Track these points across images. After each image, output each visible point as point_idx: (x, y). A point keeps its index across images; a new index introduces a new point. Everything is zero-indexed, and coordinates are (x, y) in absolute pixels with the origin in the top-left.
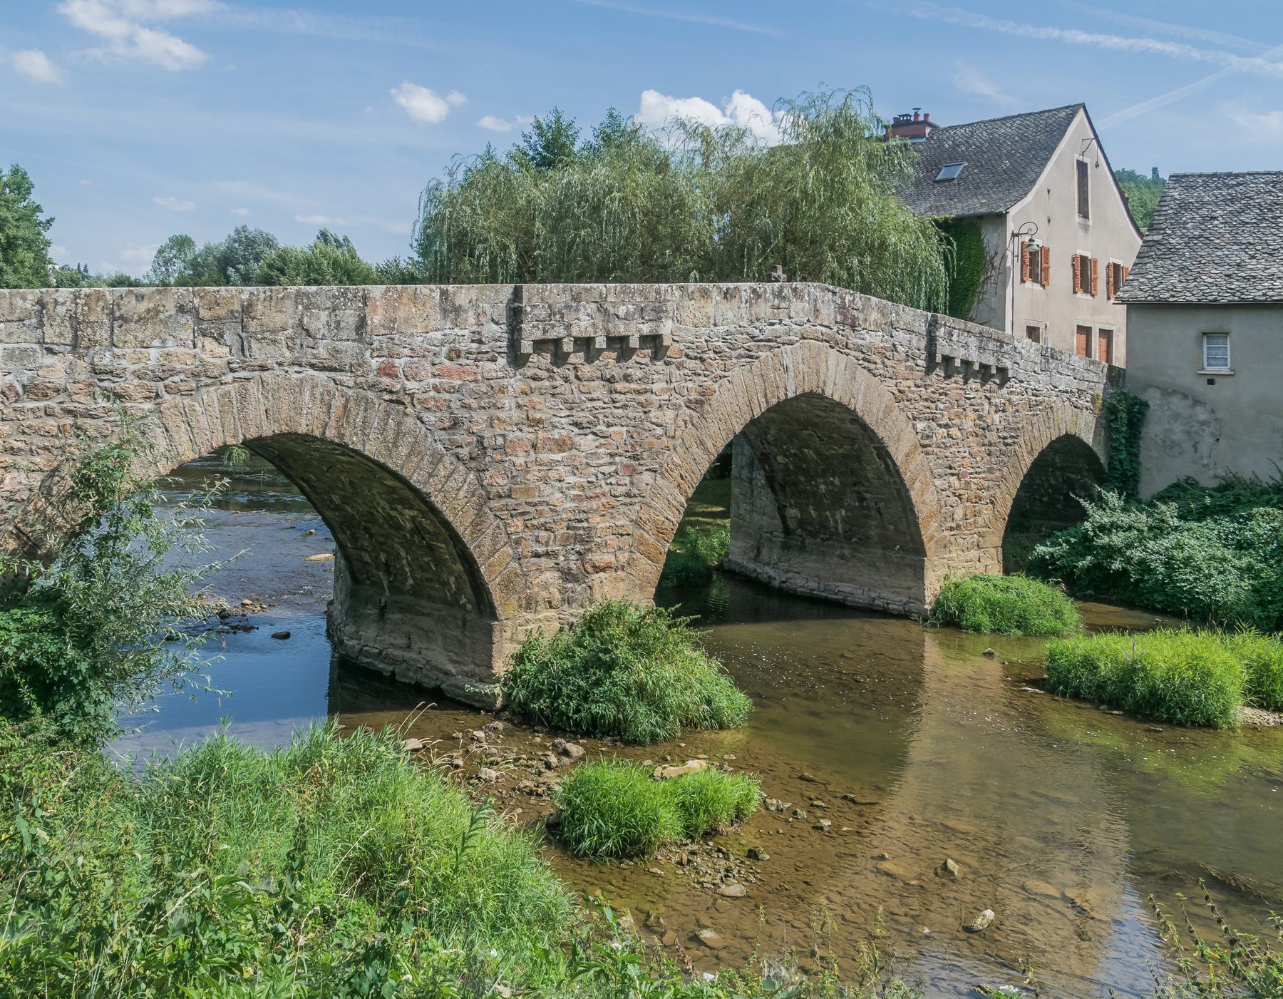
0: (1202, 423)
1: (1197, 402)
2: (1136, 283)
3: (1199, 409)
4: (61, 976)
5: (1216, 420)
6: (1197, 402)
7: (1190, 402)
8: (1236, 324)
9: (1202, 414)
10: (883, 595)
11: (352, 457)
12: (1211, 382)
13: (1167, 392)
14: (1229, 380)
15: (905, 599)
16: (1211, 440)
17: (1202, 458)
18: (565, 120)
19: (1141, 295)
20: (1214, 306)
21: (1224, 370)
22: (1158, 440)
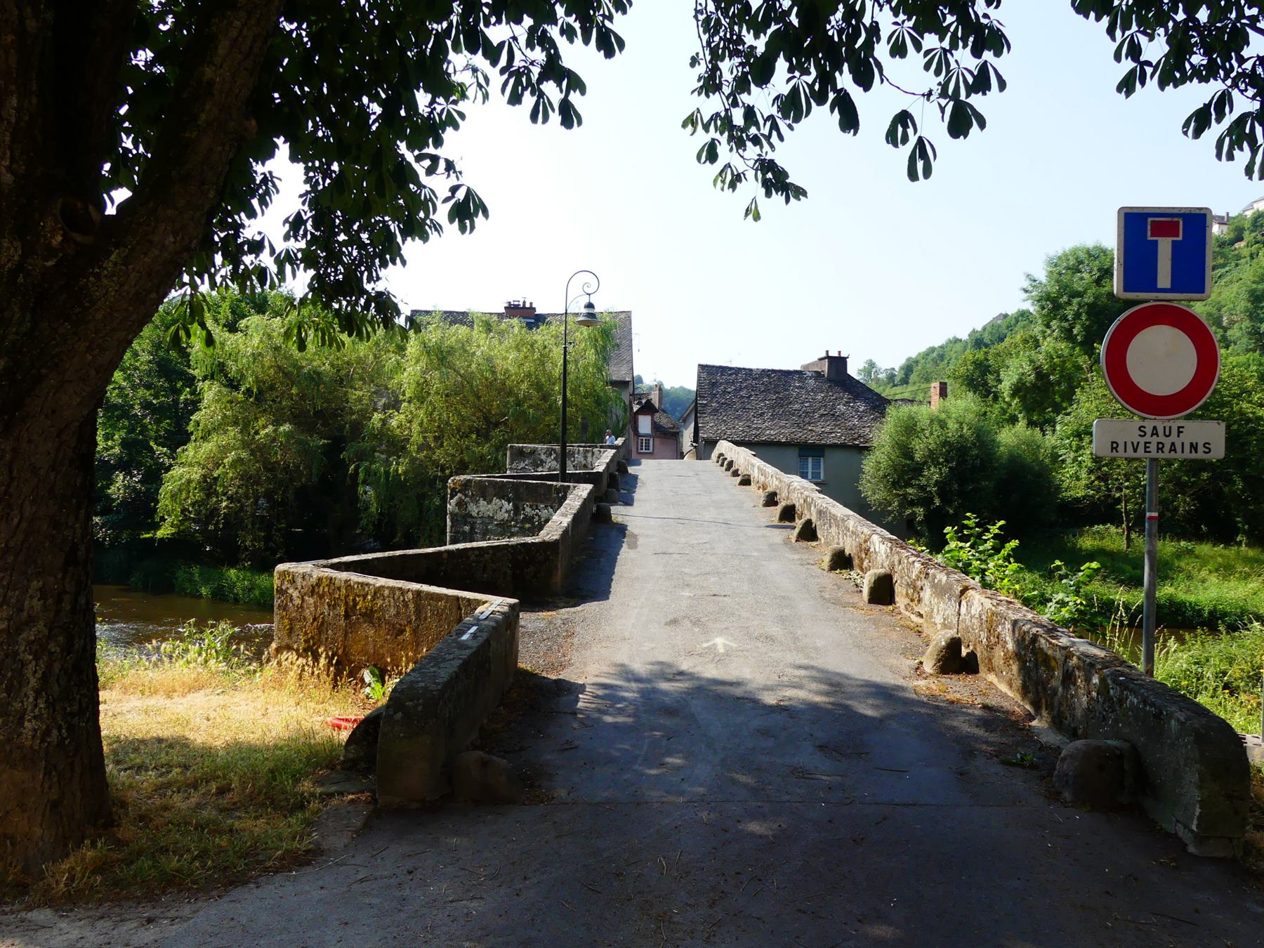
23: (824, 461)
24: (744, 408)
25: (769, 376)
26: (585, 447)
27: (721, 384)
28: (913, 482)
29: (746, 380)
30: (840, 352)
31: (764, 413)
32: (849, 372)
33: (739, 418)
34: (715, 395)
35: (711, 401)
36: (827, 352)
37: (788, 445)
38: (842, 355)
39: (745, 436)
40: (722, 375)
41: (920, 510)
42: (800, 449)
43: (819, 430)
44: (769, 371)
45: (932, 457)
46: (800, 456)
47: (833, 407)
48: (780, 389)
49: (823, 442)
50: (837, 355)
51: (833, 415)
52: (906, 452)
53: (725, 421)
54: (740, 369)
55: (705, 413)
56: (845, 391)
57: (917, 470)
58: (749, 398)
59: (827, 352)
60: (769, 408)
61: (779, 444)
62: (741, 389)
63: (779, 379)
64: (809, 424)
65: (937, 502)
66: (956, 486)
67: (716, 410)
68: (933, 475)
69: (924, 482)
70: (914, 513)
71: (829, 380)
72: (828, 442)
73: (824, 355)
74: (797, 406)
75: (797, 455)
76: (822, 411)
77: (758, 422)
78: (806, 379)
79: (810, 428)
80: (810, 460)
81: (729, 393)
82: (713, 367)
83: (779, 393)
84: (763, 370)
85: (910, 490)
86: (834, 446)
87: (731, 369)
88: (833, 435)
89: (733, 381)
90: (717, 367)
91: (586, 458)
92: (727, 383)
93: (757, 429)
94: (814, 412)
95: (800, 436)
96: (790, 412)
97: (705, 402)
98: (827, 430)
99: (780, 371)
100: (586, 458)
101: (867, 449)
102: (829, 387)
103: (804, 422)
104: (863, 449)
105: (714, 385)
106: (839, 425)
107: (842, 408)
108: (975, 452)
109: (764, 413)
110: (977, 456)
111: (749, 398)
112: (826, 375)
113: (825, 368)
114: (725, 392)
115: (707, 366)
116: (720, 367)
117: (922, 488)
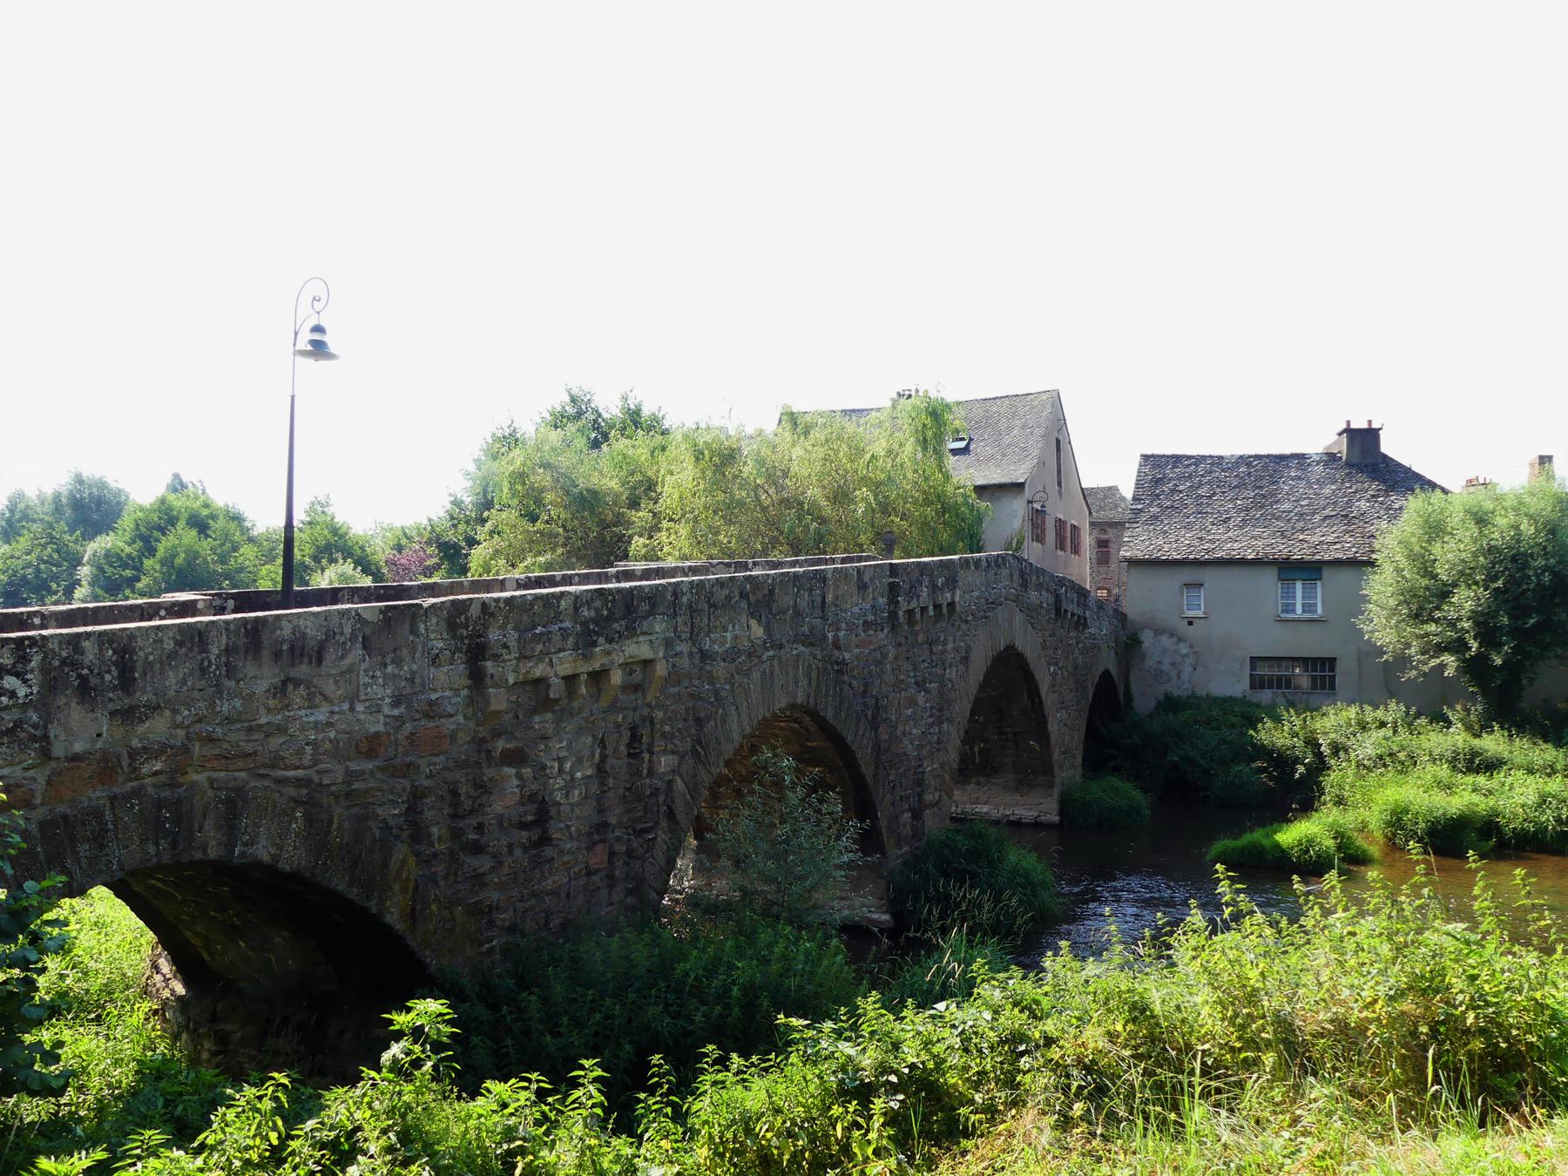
0: (1185, 656)
1: (1180, 639)
2: (1132, 544)
3: (1182, 645)
4: (1299, 474)
5: (1194, 652)
6: (1180, 639)
7: (1175, 639)
8: (1209, 576)
9: (1184, 649)
10: (1016, 812)
11: (1463, 1086)
12: (1190, 623)
13: (1159, 631)
14: (1202, 621)
15: (1036, 814)
16: (1190, 669)
17: (1183, 684)
18: (550, 409)
19: (1139, 555)
20: (1196, 563)
21: (1200, 613)
22: (1151, 670)
23: (1323, 587)
24: (1200, 513)
25: (1249, 465)
26: (660, 573)
27: (1170, 480)
28: (1437, 614)
29: (1211, 472)
30: (1370, 422)
31: (1229, 519)
32: (1382, 450)
33: (1189, 527)
34: (1158, 495)
35: (1150, 505)
36: (1348, 422)
37: (1258, 563)
38: (1374, 426)
39: (1191, 553)
40: (1174, 467)
41: (1449, 659)
42: (1280, 569)
43: (1316, 539)
44: (1250, 457)
45: (1465, 575)
46: (1280, 579)
47: (1349, 503)
48: (1264, 482)
49: (1317, 557)
50: (1365, 426)
51: (1346, 516)
52: (1426, 568)
53: (1165, 532)
54: (1204, 458)
55: (1137, 522)
56: (1374, 479)
57: (1444, 594)
58: (1210, 497)
59: (1348, 422)
60: (1240, 511)
61: (1243, 562)
62: (1200, 485)
63: (1265, 468)
64: (1302, 531)
65: (1474, 645)
66: (1505, 620)
67: (1155, 517)
68: (1465, 601)
69: (1453, 615)
70: (1442, 666)
71: (1349, 464)
72: (1327, 558)
73: (1344, 426)
74: (1286, 506)
75: (1276, 577)
76: (1327, 512)
77: (1218, 532)
78: (1309, 465)
79: (1301, 537)
80: (1299, 585)
81: (1181, 492)
82: (1163, 456)
83: (1261, 488)
84: (1241, 457)
85: (1432, 628)
86: (1337, 563)
87: (1189, 457)
88: (1338, 546)
89: (1190, 475)
90: (1168, 457)
92: (1181, 478)
93: (1212, 541)
94: (1313, 514)
95: (1281, 549)
96: (1274, 515)
97: (1140, 507)
98: (1330, 539)
99: (1268, 456)
101: (1371, 564)
102: (1347, 475)
103: (1293, 528)
104: (1362, 564)
105: (1157, 482)
106: (1352, 531)
107: (1363, 505)
108: (1540, 562)
109: (1229, 519)
110: (1546, 569)
111: (1210, 497)
112: (1344, 458)
113: (1342, 448)
114: (1173, 491)
115: (1152, 456)
116: (1173, 456)
117: (1452, 624)
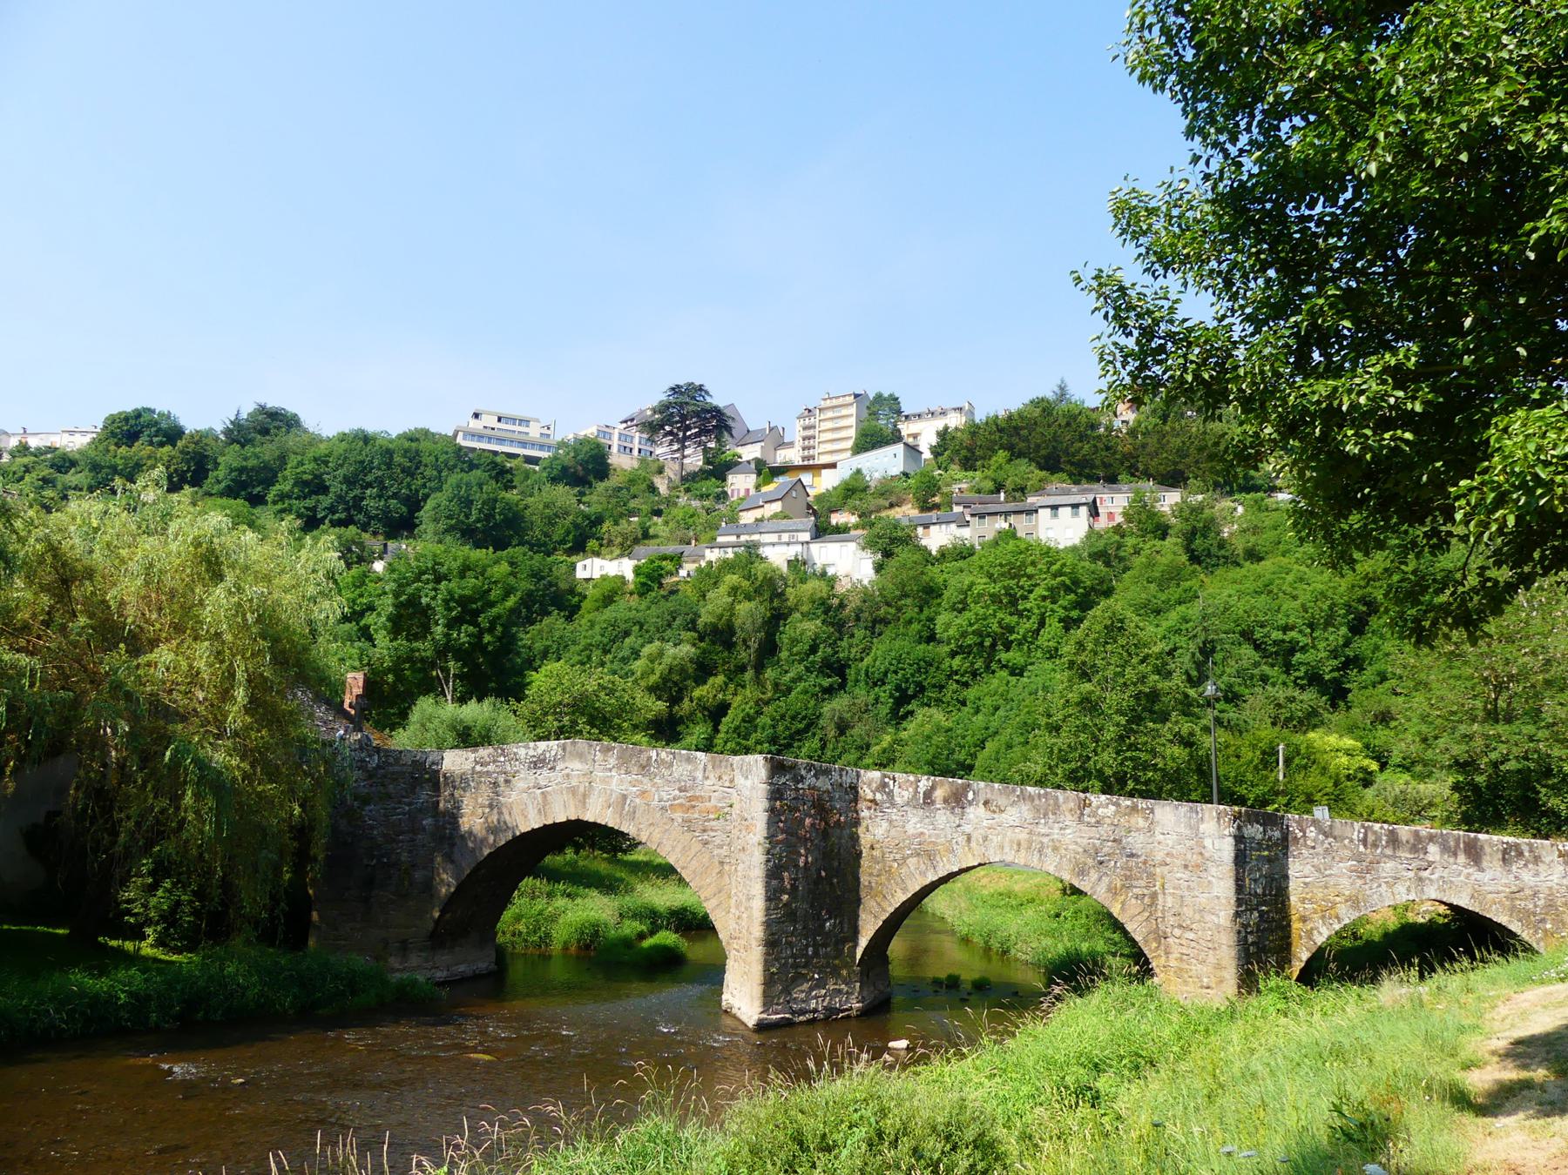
91: (841, 776)
100: (841, 776)
